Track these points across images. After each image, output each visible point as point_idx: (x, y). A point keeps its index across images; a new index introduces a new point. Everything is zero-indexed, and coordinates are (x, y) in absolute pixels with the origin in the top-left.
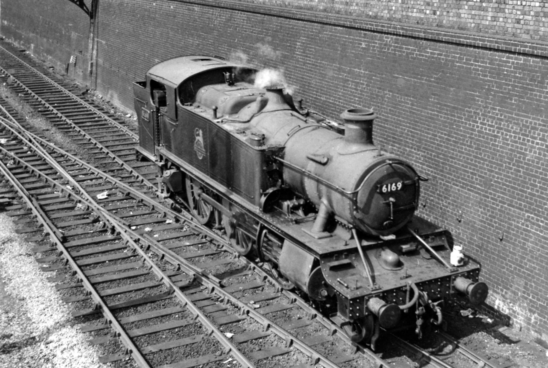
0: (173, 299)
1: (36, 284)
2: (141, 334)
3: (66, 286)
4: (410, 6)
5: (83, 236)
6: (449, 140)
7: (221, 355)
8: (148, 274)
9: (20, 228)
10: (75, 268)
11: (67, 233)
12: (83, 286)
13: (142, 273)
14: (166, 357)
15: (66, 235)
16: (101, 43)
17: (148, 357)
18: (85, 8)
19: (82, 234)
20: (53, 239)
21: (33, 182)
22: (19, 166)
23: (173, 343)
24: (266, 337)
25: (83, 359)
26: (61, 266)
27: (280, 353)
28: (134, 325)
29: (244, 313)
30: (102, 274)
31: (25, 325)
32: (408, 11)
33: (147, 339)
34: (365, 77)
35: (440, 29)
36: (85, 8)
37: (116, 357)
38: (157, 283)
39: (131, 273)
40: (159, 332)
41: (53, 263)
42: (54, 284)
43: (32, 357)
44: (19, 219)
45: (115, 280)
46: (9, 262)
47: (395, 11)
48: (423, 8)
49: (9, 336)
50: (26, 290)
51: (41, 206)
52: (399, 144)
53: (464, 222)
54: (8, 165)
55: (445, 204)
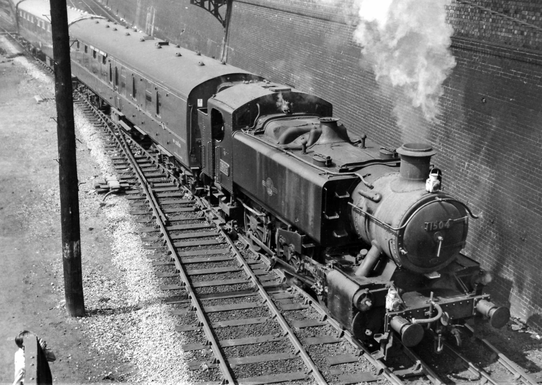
0: (249, 284)
1: (137, 258)
2: (215, 310)
3: (161, 263)
4: (500, 25)
5: (184, 222)
6: (523, 161)
7: (279, 337)
8: (232, 260)
9: (134, 210)
10: (171, 249)
11: (171, 218)
12: (174, 265)
13: (227, 259)
14: (231, 333)
15: (170, 220)
16: (231, 50)
17: (216, 331)
18: (219, 17)
19: (183, 220)
20: (158, 222)
21: (153, 172)
22: (144, 156)
23: (241, 322)
24: (322, 326)
25: (162, 326)
26: (160, 246)
27: (330, 342)
28: (210, 302)
29: (307, 303)
30: (193, 256)
31: (122, 292)
32: (497, 31)
33: (220, 316)
34: (451, 94)
35: (525, 49)
36: (219, 17)
37: (189, 328)
38: (238, 269)
39: (222, 258)
40: (231, 310)
41: (155, 242)
42: (151, 261)
43: (122, 320)
44: (135, 202)
45: (203, 262)
46: (120, 238)
47: (485, 30)
48: (512, 27)
49: (107, 300)
50: (129, 263)
51: (154, 193)
52: (476, 161)
53: (527, 242)
54: (136, 155)
55: (511, 222)
